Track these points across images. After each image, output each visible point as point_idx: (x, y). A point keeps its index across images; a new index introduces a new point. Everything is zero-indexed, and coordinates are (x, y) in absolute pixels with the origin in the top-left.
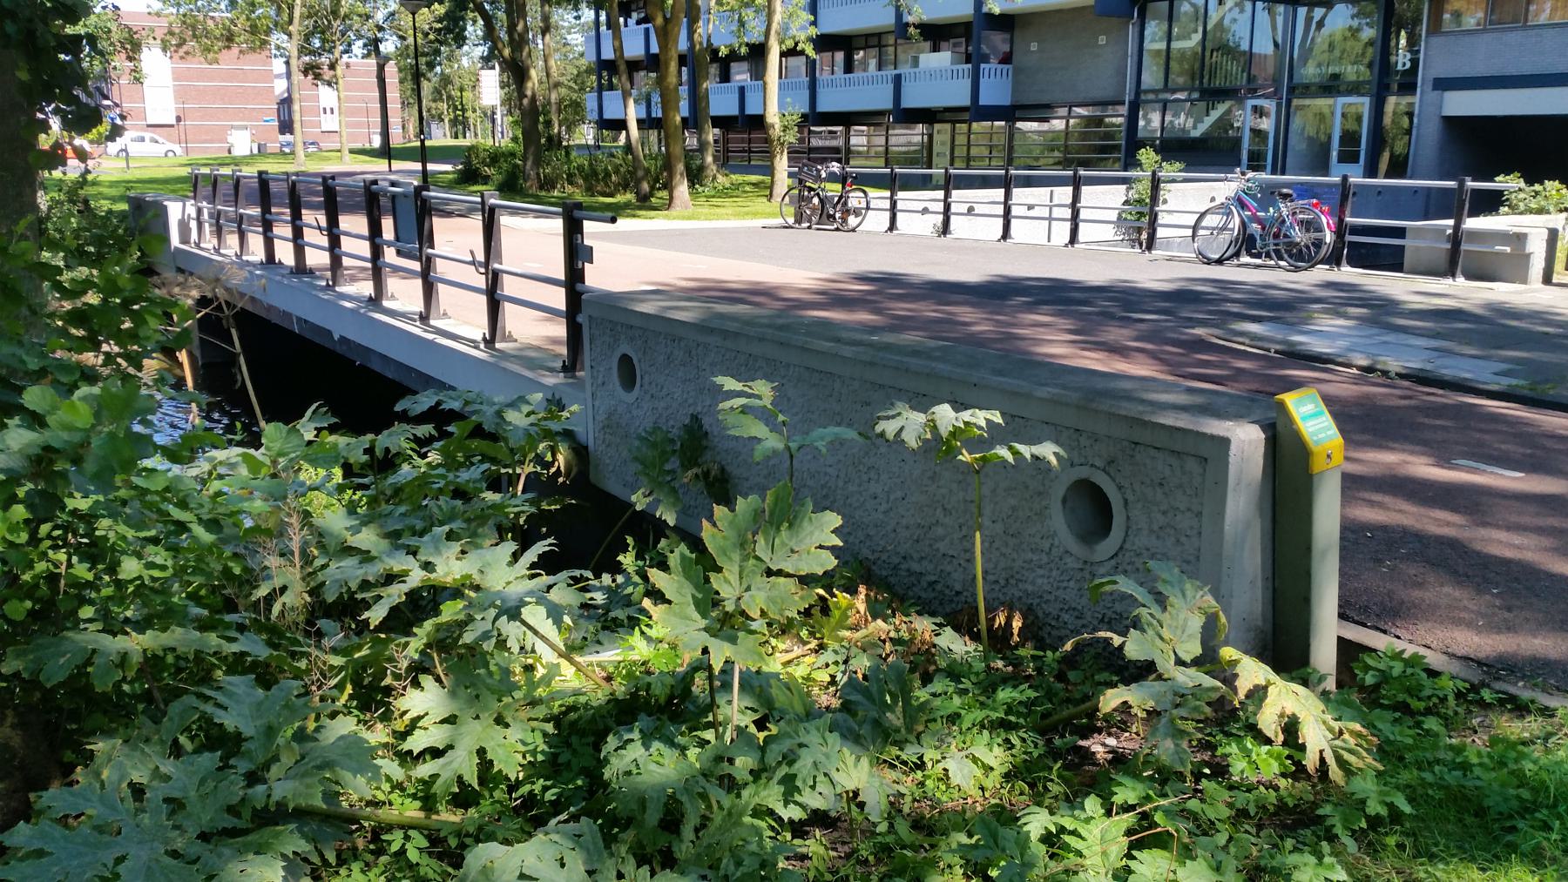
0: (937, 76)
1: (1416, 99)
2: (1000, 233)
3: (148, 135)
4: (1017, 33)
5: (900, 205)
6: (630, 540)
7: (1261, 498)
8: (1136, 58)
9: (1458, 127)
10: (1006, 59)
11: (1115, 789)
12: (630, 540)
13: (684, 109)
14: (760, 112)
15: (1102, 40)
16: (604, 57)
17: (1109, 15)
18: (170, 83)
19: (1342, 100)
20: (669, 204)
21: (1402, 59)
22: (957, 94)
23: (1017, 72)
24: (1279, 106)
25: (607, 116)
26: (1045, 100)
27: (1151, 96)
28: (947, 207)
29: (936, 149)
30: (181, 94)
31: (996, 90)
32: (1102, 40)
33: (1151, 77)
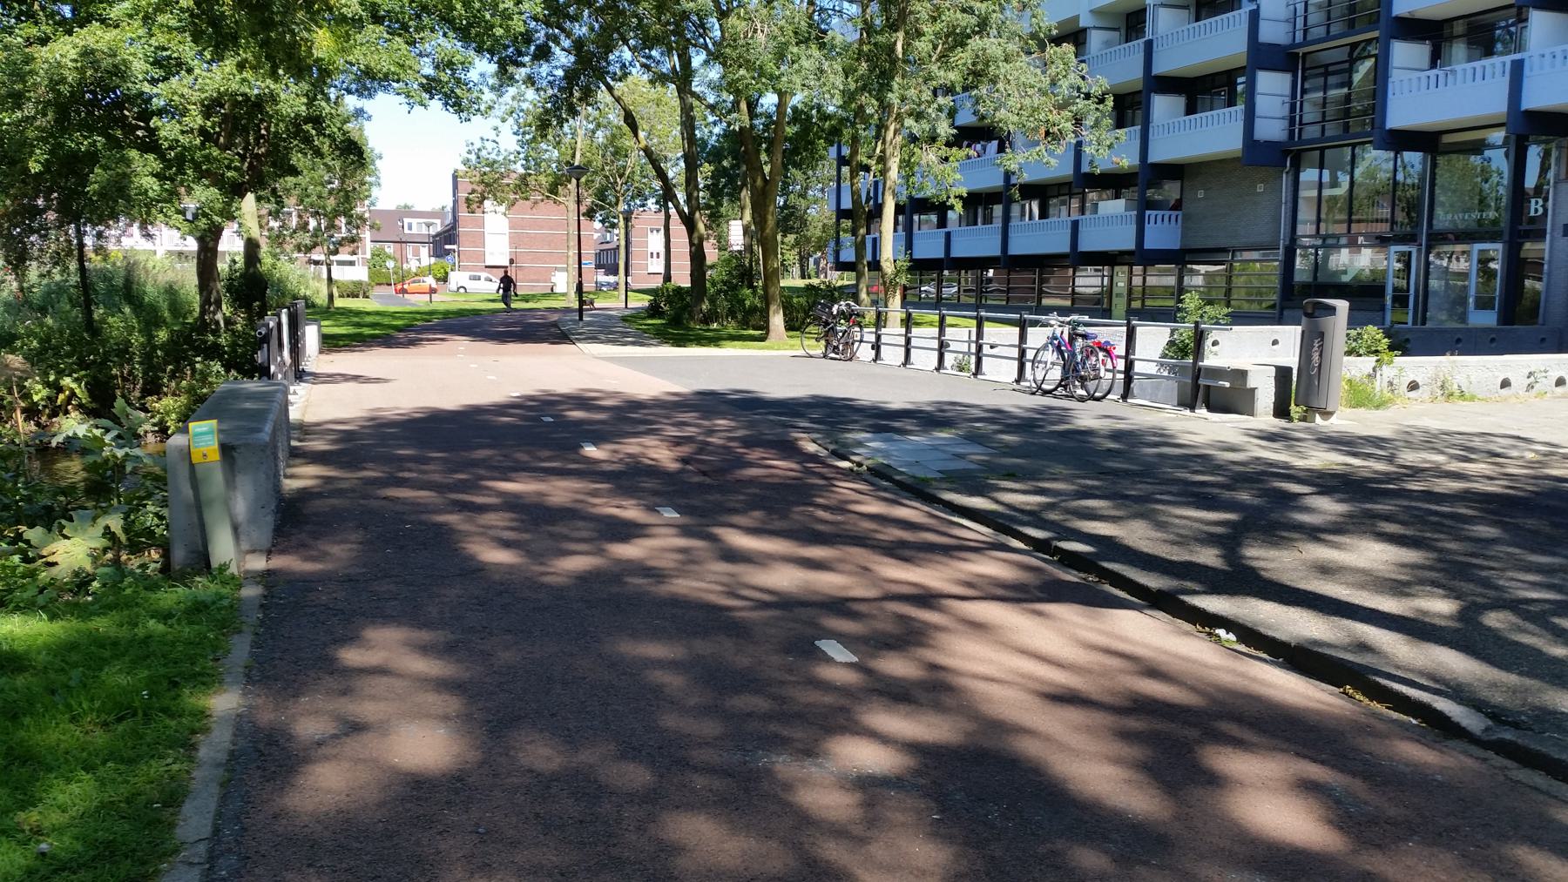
0: (1110, 222)
1: (1546, 246)
2: (1015, 376)
3: (484, 275)
4: (1186, 184)
5: (914, 342)
7: (816, 593)
8: (1290, 205)
13: (869, 257)
15: (1260, 188)
16: (843, 207)
18: (507, 230)
19: (1478, 247)
22: (1124, 240)
23: (1186, 218)
24: (1419, 251)
25: (842, 259)
26: (1222, 243)
28: (908, 341)
29: (1115, 290)
30: (515, 241)
31: (1162, 233)
32: (1260, 188)
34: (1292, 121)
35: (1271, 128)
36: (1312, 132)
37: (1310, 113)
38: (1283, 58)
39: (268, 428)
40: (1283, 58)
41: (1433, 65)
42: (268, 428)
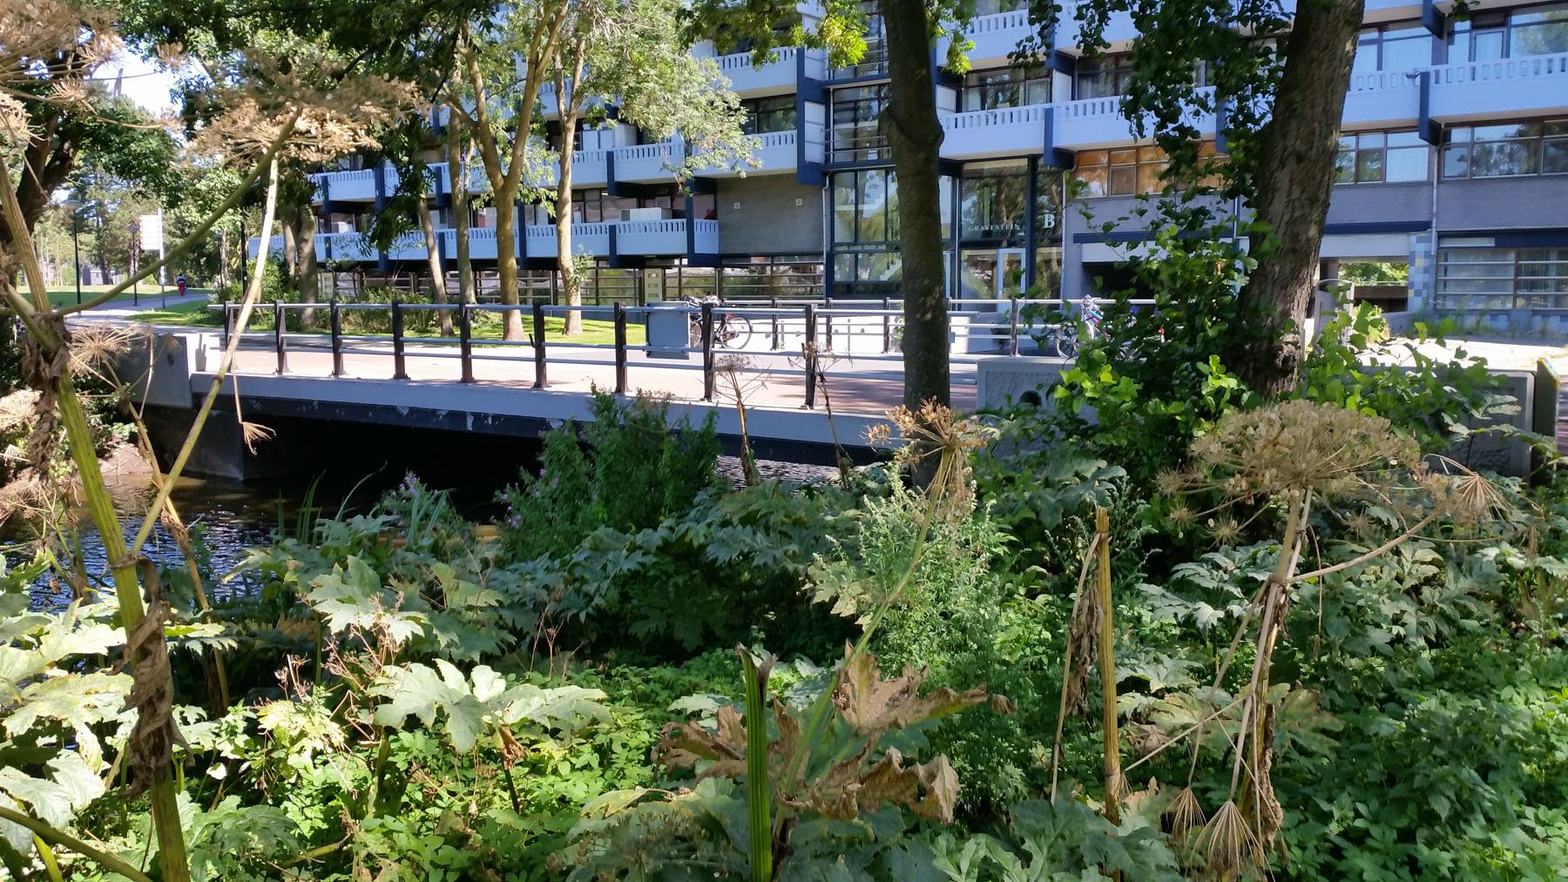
1: (1062, 249)
4: (719, 197)
6: (253, 451)
9: (1091, 269)
10: (712, 216)
11: (687, 539)
12: (253, 451)
14: (555, 255)
15: (799, 202)
17: (804, 183)
20: (1285, 523)
21: (1048, 220)
23: (722, 228)
25: (698, 250)
27: (845, 248)
31: (706, 242)
32: (799, 202)
33: (842, 235)
34: (827, 148)
35: (814, 154)
36: (841, 157)
37: (838, 141)
38: (822, 93)
39: (957, 301)
40: (822, 93)
41: (959, 109)
42: (957, 301)
